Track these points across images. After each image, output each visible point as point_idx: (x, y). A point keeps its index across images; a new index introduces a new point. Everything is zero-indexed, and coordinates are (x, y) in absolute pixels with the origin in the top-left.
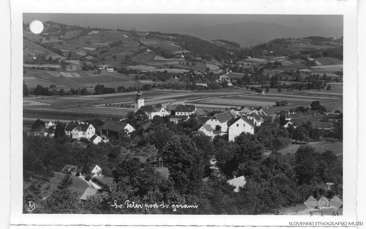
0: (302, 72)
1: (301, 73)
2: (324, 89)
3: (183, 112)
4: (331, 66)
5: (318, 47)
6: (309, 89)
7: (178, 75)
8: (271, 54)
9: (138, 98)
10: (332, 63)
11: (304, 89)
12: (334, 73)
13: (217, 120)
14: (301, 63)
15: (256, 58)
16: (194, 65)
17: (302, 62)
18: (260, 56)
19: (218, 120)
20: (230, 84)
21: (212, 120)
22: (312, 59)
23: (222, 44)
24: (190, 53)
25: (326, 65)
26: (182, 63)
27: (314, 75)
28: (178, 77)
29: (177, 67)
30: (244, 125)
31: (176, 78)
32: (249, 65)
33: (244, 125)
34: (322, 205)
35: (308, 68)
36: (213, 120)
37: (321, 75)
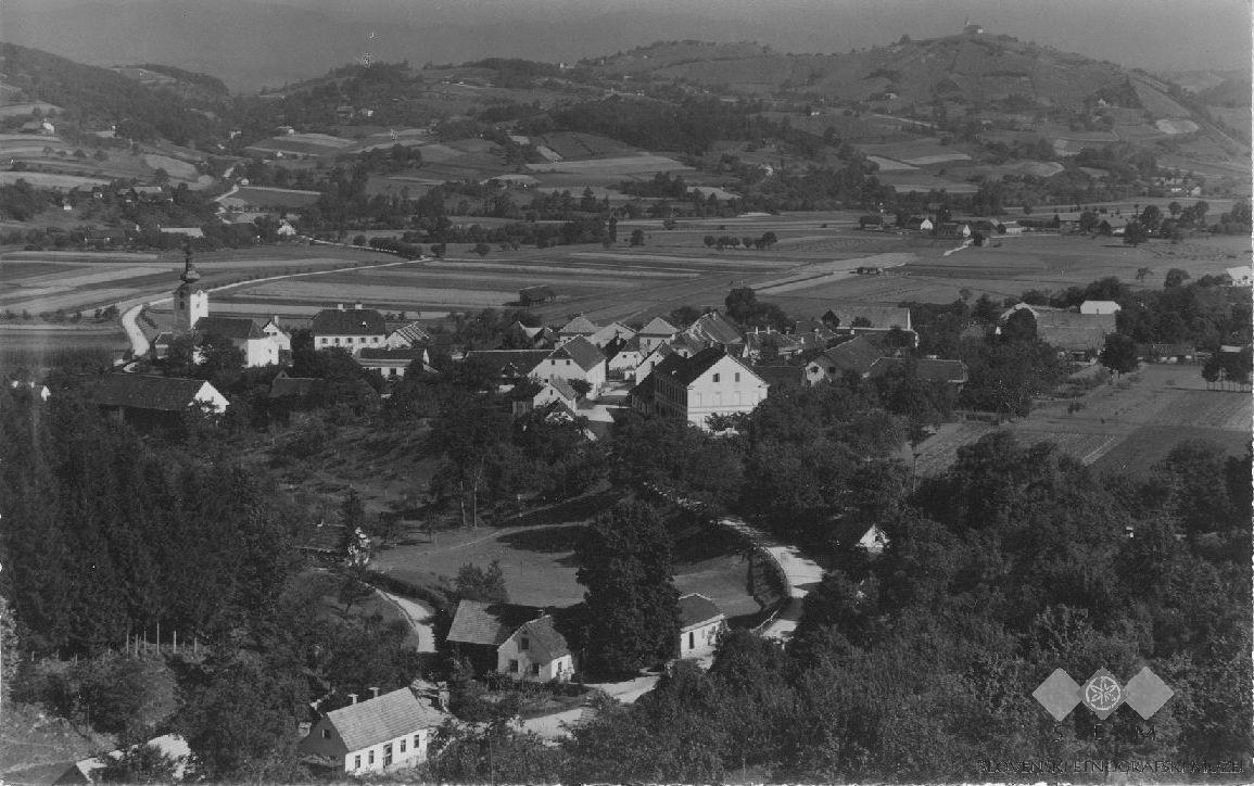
0: (509, 182)
1: (505, 187)
2: (617, 244)
3: (342, 333)
4: (592, 163)
5: (522, 97)
6: (568, 242)
7: (75, 196)
8: (367, 121)
9: (187, 289)
10: (593, 154)
11: (553, 245)
12: (612, 187)
13: (571, 361)
14: (491, 153)
15: (315, 132)
16: (101, 160)
17: (492, 151)
18: (327, 125)
19: (575, 361)
20: (287, 229)
21: (553, 363)
22: (523, 140)
23: (162, 82)
24: (63, 114)
25: (575, 159)
26: (58, 150)
27: (556, 194)
28: (73, 206)
29: (40, 165)
30: (737, 376)
31: (68, 208)
32: (295, 157)
33: (737, 377)
34: (1099, 701)
35: (517, 172)
36: (557, 361)
37: (577, 194)
